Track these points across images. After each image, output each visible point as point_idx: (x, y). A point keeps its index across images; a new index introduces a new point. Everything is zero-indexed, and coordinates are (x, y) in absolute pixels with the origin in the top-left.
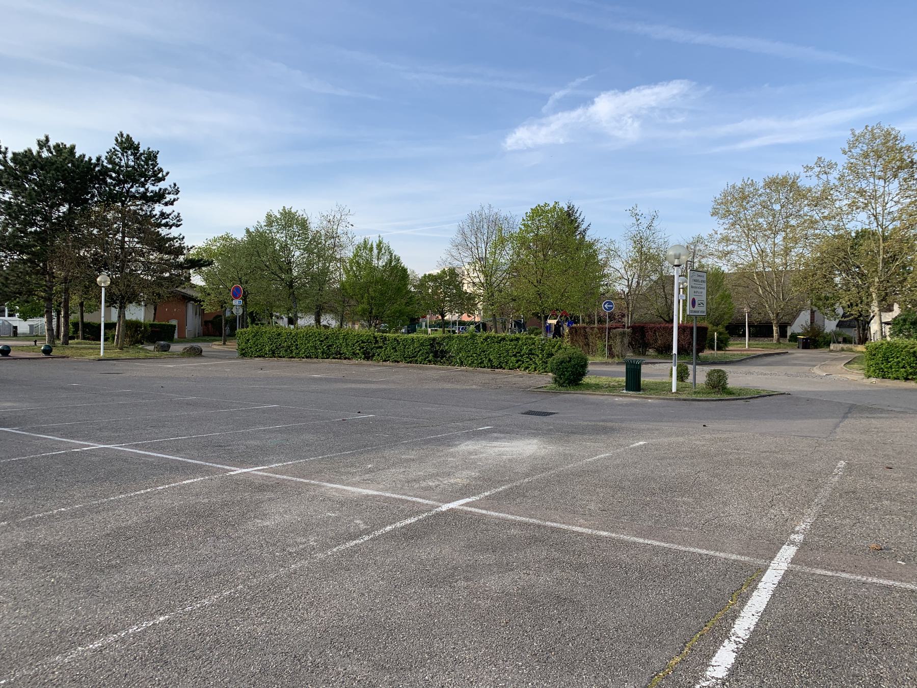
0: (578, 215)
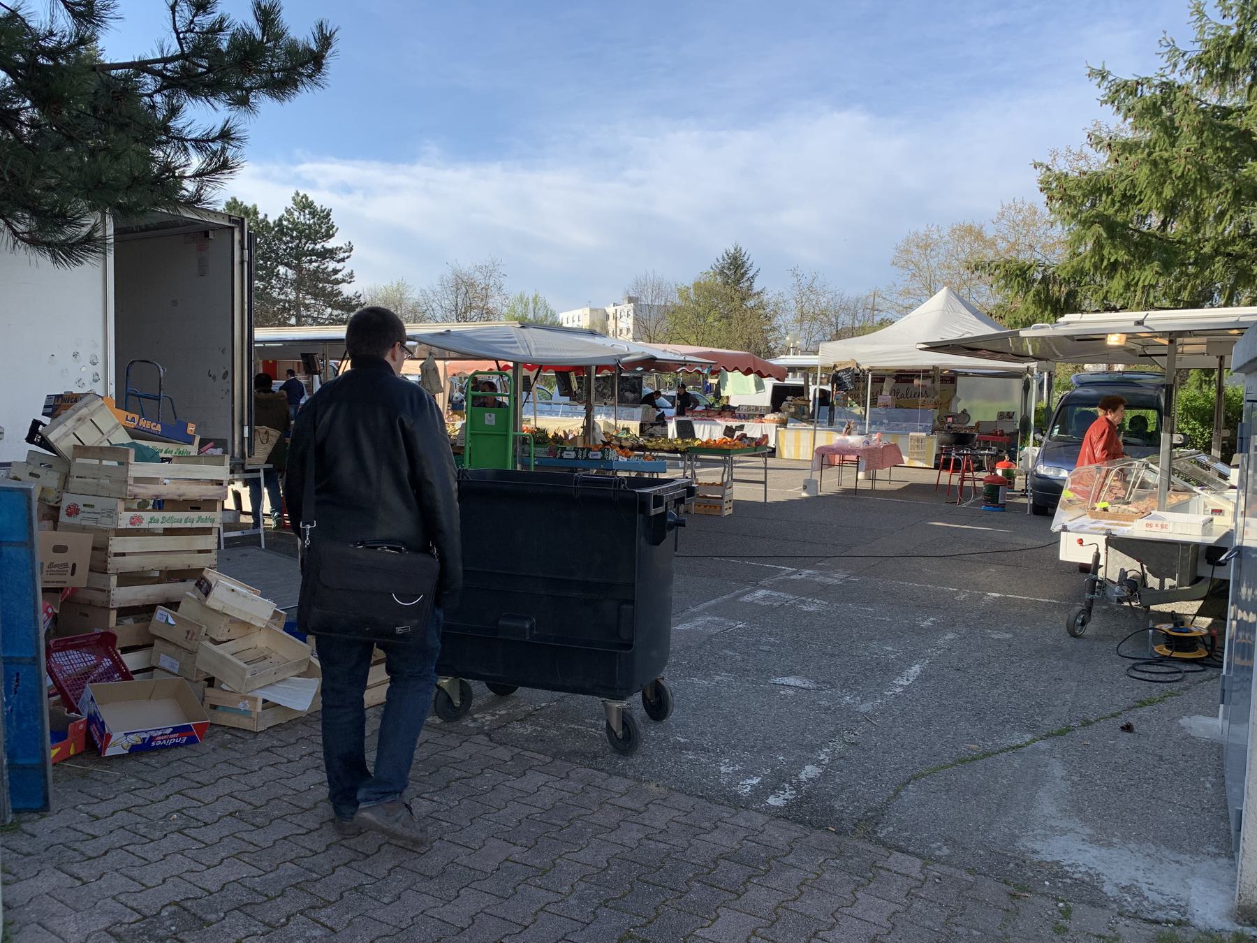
0: (746, 258)
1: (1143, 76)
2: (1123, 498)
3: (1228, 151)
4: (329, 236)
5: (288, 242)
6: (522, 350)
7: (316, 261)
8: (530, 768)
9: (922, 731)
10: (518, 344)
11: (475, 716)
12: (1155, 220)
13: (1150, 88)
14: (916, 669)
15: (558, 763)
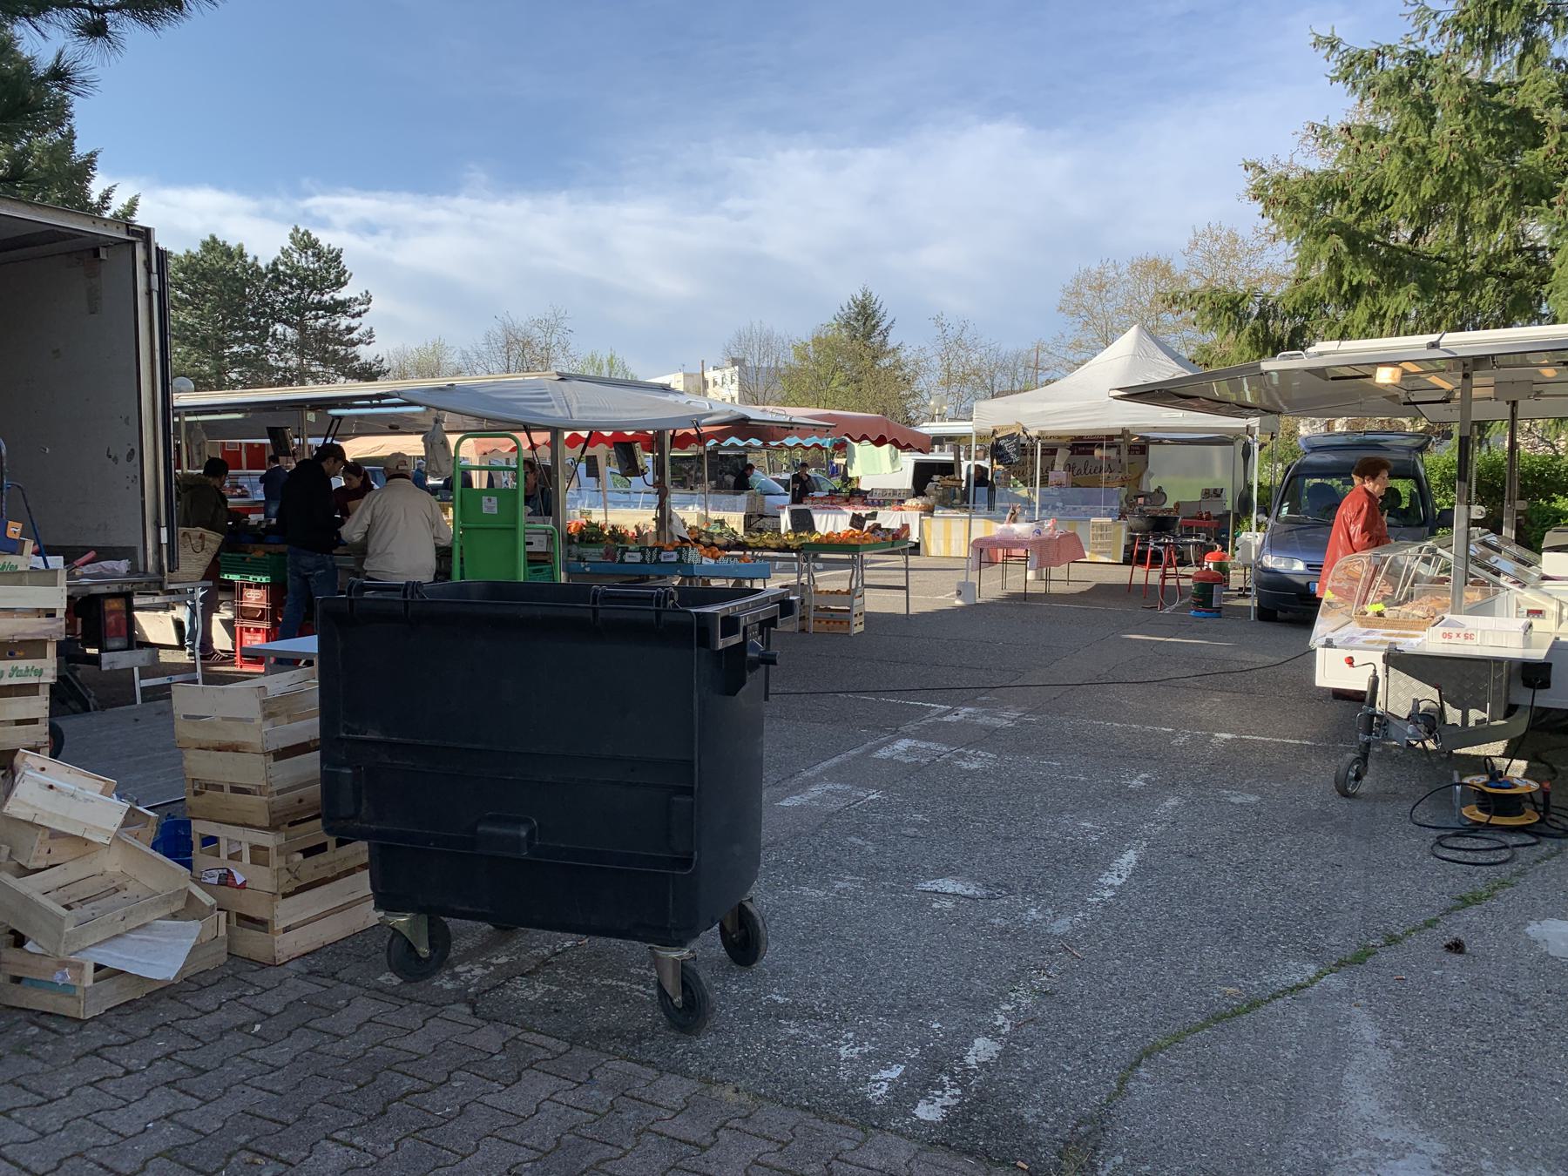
0: (877, 306)
1: (1385, 43)
2: (1392, 597)
3: (1501, 135)
4: (339, 284)
5: (286, 293)
6: (559, 411)
7: (323, 317)
8: (531, 1067)
9: (1149, 965)
10: (554, 402)
11: (459, 969)
12: (1405, 234)
13: (1394, 59)
14: (1129, 858)
15: (578, 1052)
